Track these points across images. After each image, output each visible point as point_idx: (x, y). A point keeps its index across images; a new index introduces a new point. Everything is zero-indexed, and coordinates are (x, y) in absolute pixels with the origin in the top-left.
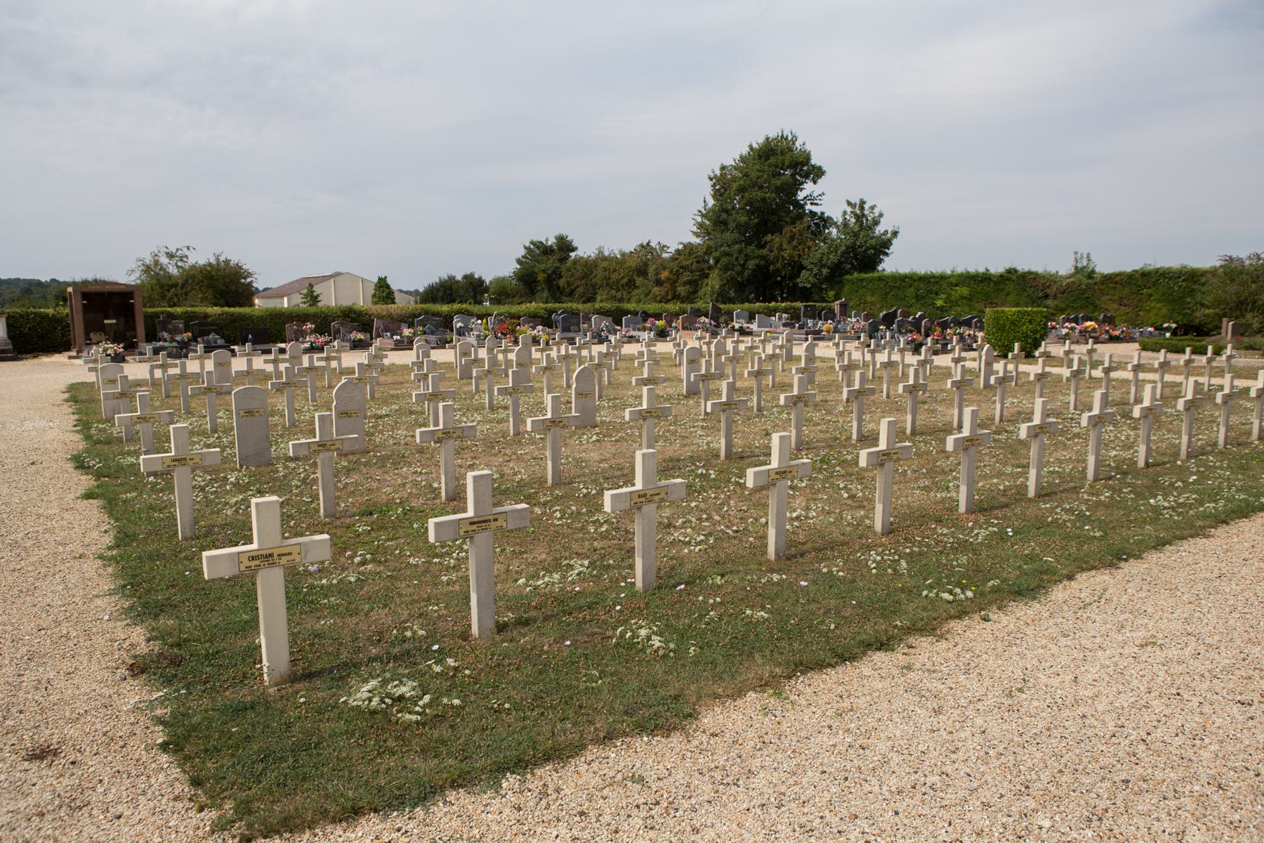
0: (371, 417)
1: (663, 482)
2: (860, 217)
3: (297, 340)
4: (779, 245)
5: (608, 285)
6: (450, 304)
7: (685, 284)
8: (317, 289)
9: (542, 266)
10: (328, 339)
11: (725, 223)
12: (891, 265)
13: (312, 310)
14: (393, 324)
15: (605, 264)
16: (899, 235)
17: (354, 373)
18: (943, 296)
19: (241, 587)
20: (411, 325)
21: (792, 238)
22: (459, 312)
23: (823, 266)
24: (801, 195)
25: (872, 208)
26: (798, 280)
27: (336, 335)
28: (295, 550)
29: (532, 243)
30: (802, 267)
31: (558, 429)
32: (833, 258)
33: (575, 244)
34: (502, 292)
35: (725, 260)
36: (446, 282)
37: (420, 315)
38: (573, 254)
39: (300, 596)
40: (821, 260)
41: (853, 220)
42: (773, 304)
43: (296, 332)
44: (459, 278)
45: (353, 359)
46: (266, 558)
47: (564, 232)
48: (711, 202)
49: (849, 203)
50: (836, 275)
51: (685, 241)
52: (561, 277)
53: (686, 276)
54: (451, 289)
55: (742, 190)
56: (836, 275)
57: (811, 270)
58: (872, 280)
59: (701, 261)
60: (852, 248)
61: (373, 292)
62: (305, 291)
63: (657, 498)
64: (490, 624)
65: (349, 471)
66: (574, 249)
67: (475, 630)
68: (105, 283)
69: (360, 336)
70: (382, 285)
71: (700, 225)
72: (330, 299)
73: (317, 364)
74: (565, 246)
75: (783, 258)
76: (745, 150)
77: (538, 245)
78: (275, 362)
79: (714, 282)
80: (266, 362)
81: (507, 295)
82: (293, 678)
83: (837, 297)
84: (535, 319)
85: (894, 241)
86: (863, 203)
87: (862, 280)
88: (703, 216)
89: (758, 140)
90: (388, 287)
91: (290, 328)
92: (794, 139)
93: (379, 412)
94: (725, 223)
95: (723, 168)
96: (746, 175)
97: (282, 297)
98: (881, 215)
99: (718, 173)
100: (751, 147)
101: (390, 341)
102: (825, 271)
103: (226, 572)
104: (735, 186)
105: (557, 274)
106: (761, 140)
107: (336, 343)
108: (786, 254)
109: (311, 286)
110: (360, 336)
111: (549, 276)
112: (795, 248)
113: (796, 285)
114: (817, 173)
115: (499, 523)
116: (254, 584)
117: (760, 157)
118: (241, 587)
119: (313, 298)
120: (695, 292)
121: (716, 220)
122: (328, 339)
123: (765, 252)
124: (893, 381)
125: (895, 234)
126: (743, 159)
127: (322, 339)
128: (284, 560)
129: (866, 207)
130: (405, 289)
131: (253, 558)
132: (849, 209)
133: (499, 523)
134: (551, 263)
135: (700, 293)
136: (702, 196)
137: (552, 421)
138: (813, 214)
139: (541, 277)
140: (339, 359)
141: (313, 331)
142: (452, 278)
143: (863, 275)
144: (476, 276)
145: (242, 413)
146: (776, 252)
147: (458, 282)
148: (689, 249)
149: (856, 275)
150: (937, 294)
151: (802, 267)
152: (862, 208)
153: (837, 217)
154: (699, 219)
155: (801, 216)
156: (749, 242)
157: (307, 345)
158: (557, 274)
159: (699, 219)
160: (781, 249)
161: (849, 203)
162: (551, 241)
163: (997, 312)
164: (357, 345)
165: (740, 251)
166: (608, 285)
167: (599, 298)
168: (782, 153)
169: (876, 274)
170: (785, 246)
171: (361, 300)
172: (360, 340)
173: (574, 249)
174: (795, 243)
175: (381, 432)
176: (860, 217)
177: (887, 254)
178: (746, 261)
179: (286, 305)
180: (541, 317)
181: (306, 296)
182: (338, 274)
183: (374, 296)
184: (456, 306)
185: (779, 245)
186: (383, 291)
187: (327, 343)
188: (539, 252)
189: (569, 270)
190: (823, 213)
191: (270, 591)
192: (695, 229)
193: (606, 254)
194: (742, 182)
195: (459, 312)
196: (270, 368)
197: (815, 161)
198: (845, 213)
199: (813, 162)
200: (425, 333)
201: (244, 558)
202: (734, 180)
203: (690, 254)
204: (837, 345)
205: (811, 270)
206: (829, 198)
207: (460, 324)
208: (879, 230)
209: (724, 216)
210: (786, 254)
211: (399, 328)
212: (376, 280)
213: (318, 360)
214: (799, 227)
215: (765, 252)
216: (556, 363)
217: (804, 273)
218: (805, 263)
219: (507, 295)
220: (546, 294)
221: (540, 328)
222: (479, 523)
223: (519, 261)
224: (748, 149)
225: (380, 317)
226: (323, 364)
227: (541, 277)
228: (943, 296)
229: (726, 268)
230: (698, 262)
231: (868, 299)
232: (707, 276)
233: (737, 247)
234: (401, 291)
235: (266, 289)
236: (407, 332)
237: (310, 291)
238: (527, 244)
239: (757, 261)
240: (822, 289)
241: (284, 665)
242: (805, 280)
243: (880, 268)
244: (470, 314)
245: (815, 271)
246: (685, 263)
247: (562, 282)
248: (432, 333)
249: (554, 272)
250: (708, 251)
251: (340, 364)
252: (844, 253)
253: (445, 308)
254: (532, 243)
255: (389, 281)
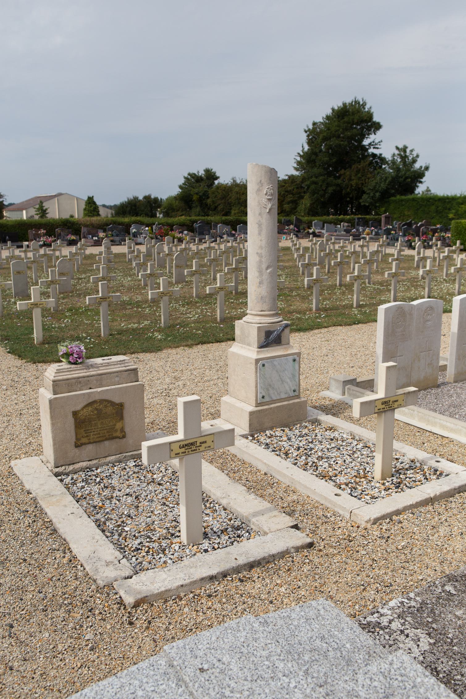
0: (76, 279)
1: (172, 289)
2: (404, 158)
3: (35, 240)
4: (349, 177)
5: (239, 203)
6: (137, 213)
7: (289, 203)
8: (46, 205)
9: (196, 190)
10: (53, 239)
11: (314, 161)
12: (420, 189)
13: (43, 221)
14: (94, 229)
15: (237, 189)
16: (430, 169)
17: (67, 256)
18: (454, 211)
19: (27, 314)
20: (105, 231)
21: (358, 171)
22: (135, 222)
23: (377, 191)
24: (366, 142)
25: (412, 151)
26: (361, 201)
27: (58, 237)
28: (44, 303)
29: (189, 174)
30: (364, 192)
31: (153, 278)
32: (383, 186)
33: (218, 174)
34: (171, 207)
35: (313, 187)
36: (132, 201)
37: (110, 224)
38: (216, 182)
39: (45, 312)
40: (375, 187)
41: (399, 160)
42: (342, 216)
43: (34, 235)
44: (141, 198)
45: (67, 251)
46: (36, 305)
47: (210, 167)
48: (306, 148)
49: (397, 148)
50: (385, 196)
51: (289, 174)
52: (208, 198)
53: (289, 198)
54: (135, 205)
55: (325, 139)
56: (385, 196)
57: (369, 194)
58: (408, 200)
59: (300, 187)
60: (397, 177)
61: (84, 207)
62: (37, 206)
63: (168, 294)
64: (107, 333)
65: (64, 298)
66: (217, 178)
67: (102, 335)
68: (458, 344)
69: (73, 237)
70: (91, 202)
71: (299, 163)
72: (55, 213)
73: (48, 252)
74: (211, 176)
75: (352, 186)
76: (329, 112)
77: (193, 176)
78: (25, 252)
79: (306, 202)
80: (20, 252)
81: (173, 210)
82: (43, 343)
83: (385, 212)
84: (184, 226)
85: (427, 173)
86: (405, 148)
87: (402, 200)
88: (301, 156)
89: (337, 104)
90: (94, 203)
91: (31, 233)
92: (364, 104)
93: (80, 277)
94: (314, 161)
95: (314, 124)
96: (329, 129)
97: (21, 210)
98: (418, 156)
99: (311, 127)
100: (333, 110)
101: (92, 241)
102: (378, 194)
103: (24, 308)
104: (321, 136)
105: (206, 195)
106: (340, 104)
107: (58, 242)
108: (353, 183)
109: (41, 203)
110: (73, 237)
111: (200, 197)
112: (359, 178)
113: (360, 203)
114: (377, 126)
115: (110, 299)
116: (32, 314)
117: (339, 117)
118: (27, 314)
119: (43, 212)
120: (295, 208)
121: (308, 160)
122: (53, 239)
123: (339, 181)
124: (449, 266)
125: (427, 168)
126: (328, 117)
127: (50, 239)
128: (41, 306)
129: (408, 151)
130: (107, 204)
131: (32, 305)
132: (397, 152)
133: (110, 299)
134: (202, 188)
135: (298, 209)
136: (299, 144)
137: (150, 274)
138: (374, 155)
139: (195, 197)
140: (60, 251)
141: (44, 235)
142: (136, 199)
143: (403, 197)
144: (152, 197)
145: (15, 273)
146: (347, 181)
147: (140, 201)
148: (292, 178)
149: (398, 197)
150: (449, 209)
151: (364, 192)
152: (405, 151)
153: (388, 156)
154: (299, 159)
155: (365, 157)
156: (329, 174)
157: (41, 243)
158: (206, 195)
159: (299, 159)
160: (350, 179)
161: (397, 148)
162: (202, 173)
163: (457, 223)
164: (72, 243)
165: (323, 181)
166: (239, 203)
167: (233, 212)
168: (353, 114)
169: (410, 197)
170: (353, 178)
171: (76, 212)
172: (73, 240)
173: (217, 178)
174: (359, 175)
175: (80, 285)
176: (404, 158)
177: (421, 182)
178: (327, 187)
179: (25, 218)
180: (187, 226)
181: (38, 209)
182: (60, 195)
183: (85, 210)
184: (134, 218)
185: (349, 177)
186: (91, 206)
187: (55, 241)
188: (193, 181)
189: (213, 193)
190: (381, 155)
191: (37, 314)
192: (295, 165)
193: (238, 182)
194: (325, 134)
195: (135, 222)
196: (23, 255)
197: (376, 119)
198: (394, 155)
199: (374, 120)
200: (113, 236)
201: (29, 304)
202: (321, 131)
203: (292, 182)
204: (312, 241)
205: (369, 194)
206: (384, 144)
207: (134, 230)
208: (417, 166)
209: (313, 157)
210: (353, 183)
211: (97, 232)
212: (86, 199)
213: (49, 251)
214: (363, 164)
215: (339, 181)
216: (136, 249)
217: (365, 196)
218: (365, 189)
219: (173, 210)
220: (198, 209)
221: (186, 232)
222: (103, 298)
223: (180, 187)
224: (331, 111)
225: (86, 226)
226: (52, 252)
227: (195, 197)
228: (454, 211)
229: (313, 193)
230: (297, 188)
231: (406, 213)
232: (302, 197)
233: (321, 178)
234: (104, 206)
235: (10, 205)
236: (101, 235)
237: (40, 205)
238: (186, 175)
239: (334, 188)
240: (376, 207)
241: (41, 339)
242: (365, 200)
243: (416, 192)
244: (142, 223)
245: (372, 194)
246: (289, 189)
247: (209, 201)
248: (117, 236)
249: (204, 194)
250: (304, 179)
251: (61, 253)
252: (390, 182)
253: (126, 220)
254: (189, 174)
255: (95, 199)
